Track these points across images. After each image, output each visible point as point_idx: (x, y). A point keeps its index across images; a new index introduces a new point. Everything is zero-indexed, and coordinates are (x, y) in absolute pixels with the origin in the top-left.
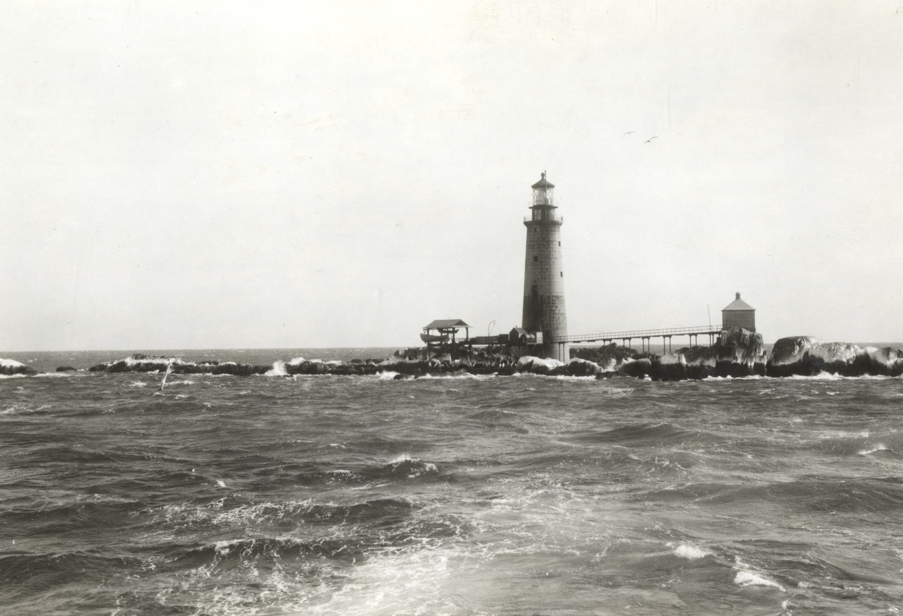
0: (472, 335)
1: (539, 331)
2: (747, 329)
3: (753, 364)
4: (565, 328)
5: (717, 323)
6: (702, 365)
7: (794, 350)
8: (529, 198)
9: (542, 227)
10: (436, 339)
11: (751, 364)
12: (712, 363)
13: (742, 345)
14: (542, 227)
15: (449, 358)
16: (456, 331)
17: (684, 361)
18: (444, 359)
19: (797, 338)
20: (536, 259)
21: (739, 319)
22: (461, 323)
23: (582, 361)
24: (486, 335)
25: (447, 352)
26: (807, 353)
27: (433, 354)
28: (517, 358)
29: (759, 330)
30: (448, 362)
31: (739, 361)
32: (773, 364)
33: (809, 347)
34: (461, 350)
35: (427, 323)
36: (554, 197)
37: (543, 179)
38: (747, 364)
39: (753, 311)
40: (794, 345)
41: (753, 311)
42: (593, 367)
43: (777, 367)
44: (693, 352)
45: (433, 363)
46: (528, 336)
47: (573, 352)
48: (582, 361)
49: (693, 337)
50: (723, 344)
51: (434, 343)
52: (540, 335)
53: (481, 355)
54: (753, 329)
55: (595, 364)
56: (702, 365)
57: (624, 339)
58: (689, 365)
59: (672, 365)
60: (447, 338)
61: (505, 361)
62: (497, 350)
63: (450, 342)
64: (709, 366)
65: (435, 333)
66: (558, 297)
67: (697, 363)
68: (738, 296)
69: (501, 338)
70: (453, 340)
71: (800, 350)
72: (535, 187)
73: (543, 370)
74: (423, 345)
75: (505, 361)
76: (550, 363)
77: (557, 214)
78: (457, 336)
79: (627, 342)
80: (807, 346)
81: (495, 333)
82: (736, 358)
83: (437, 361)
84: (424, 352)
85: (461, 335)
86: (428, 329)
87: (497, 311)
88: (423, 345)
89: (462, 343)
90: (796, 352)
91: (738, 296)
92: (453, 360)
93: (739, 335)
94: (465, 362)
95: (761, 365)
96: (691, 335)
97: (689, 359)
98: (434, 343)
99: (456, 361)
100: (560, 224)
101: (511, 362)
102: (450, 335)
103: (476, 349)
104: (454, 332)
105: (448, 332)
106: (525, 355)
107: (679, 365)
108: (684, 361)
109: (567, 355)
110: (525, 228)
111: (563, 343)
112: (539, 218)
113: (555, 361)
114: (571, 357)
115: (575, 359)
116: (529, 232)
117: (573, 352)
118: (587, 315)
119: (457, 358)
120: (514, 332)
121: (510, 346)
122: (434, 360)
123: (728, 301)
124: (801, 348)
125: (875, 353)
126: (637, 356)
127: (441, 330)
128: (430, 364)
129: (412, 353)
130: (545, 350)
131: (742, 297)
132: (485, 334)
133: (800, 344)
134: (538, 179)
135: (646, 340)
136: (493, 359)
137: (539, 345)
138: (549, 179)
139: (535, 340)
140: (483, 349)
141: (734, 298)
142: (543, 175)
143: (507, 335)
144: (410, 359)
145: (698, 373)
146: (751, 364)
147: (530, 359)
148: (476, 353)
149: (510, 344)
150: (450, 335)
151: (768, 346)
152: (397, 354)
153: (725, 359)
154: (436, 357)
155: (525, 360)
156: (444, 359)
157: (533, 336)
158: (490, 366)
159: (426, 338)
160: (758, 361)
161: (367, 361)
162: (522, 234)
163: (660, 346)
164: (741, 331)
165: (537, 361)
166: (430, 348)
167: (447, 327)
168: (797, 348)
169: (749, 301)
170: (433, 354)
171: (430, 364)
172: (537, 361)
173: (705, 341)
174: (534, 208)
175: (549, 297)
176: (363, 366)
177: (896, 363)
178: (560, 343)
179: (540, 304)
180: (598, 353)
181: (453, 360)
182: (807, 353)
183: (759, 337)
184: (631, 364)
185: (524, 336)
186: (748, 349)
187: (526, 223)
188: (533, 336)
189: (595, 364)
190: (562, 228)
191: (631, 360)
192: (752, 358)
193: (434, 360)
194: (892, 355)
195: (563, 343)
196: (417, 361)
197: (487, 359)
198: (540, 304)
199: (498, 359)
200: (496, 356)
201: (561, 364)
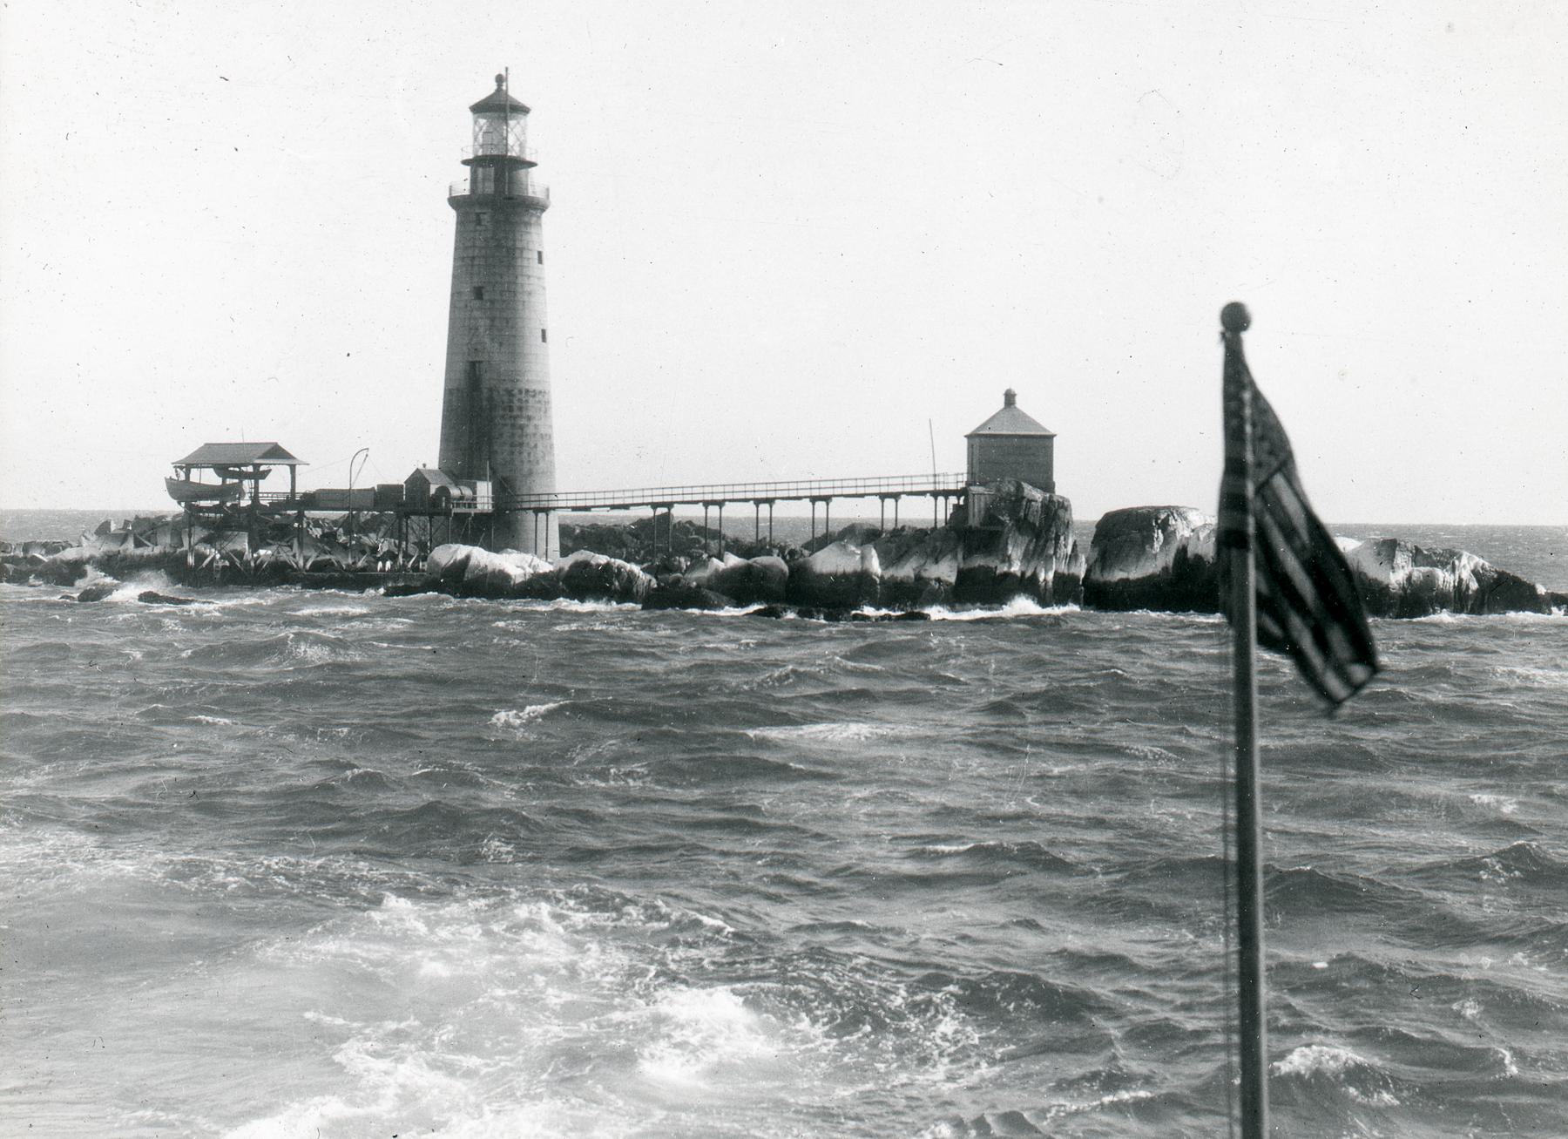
0: (306, 485)
1: (482, 478)
2: (1035, 485)
3: (1051, 575)
4: (549, 473)
5: (954, 467)
6: (918, 578)
7: (1150, 540)
8: (465, 137)
9: (496, 212)
10: (210, 492)
11: (1046, 576)
12: (945, 571)
13: (1023, 525)
14: (496, 212)
15: (242, 543)
16: (264, 475)
17: (875, 566)
18: (230, 547)
19: (1158, 510)
20: (478, 293)
21: (1011, 462)
22: (276, 453)
23: (603, 559)
24: (343, 485)
25: (240, 528)
26: (1183, 550)
27: (200, 533)
28: (424, 549)
29: (1063, 487)
30: (240, 554)
31: (1016, 568)
32: (1097, 576)
33: (1187, 533)
34: (274, 523)
35: (184, 453)
36: (522, 138)
37: (499, 90)
38: (1035, 576)
39: (1050, 438)
40: (1151, 530)
41: (1050, 438)
42: (631, 577)
43: (1106, 584)
44: (898, 542)
45: (200, 557)
46: (455, 492)
47: (572, 538)
48: (603, 559)
49: (889, 502)
50: (974, 521)
51: (203, 503)
52: (484, 489)
53: (329, 538)
54: (1048, 486)
55: (636, 569)
56: (918, 578)
57: (707, 504)
58: (887, 575)
59: (845, 575)
60: (237, 491)
61: (392, 556)
62: (366, 528)
63: (245, 502)
64: (938, 580)
65: (210, 478)
66: (535, 394)
67: (906, 571)
68: (1010, 398)
69: (384, 496)
70: (255, 498)
71: (1166, 542)
72: (479, 109)
73: (495, 586)
74: (173, 508)
75: (392, 556)
76: (514, 564)
77: (535, 182)
78: (264, 486)
79: (714, 511)
80: (1182, 531)
81: (369, 479)
82: (1007, 560)
83: (211, 553)
84: (177, 528)
85: (276, 483)
86: (187, 466)
87: (381, 428)
88: (173, 508)
89: (277, 506)
90: (1157, 546)
91: (1010, 398)
92: (254, 549)
93: (1018, 498)
94: (285, 556)
95: (1073, 579)
96: (883, 496)
97: (888, 560)
98: (203, 503)
99: (262, 552)
100: (543, 208)
101: (407, 556)
102: (247, 485)
103: (317, 523)
104: (259, 475)
105: (243, 476)
106: (444, 541)
107: (863, 577)
108: (875, 566)
109: (555, 544)
110: (451, 216)
111: (546, 510)
112: (490, 188)
113: (529, 557)
114: (565, 552)
115: (582, 555)
116: (461, 223)
117: (572, 538)
118: (602, 446)
119: (267, 545)
120: (418, 480)
121: (407, 516)
122: (201, 548)
123: (982, 410)
124: (1169, 536)
125: (1357, 552)
126: (745, 551)
127: (222, 470)
128: (191, 560)
129: (146, 528)
130: (499, 528)
131: (1020, 403)
132: (339, 482)
133: (1164, 526)
134: (487, 89)
135: (821, 505)
136: (362, 550)
137: (482, 517)
138: (517, 91)
139: (472, 502)
140: (335, 522)
141: (1002, 399)
142: (500, 79)
143: (398, 488)
144: (138, 544)
145: (907, 597)
146: (1046, 576)
147: (461, 551)
148: (317, 532)
149: (406, 505)
150: (247, 485)
151: (1084, 525)
152: (103, 530)
153: (978, 561)
154: (208, 541)
155: (448, 554)
156: (230, 547)
157: (467, 492)
158: (352, 569)
159: (179, 490)
160: (1063, 569)
161: (26, 547)
162: (439, 234)
163: (803, 521)
164: (1019, 488)
165: (482, 557)
166: (193, 517)
167: (240, 463)
168: (1159, 535)
169: (1039, 411)
170: (200, 533)
171: (191, 560)
172: (482, 557)
173: (923, 513)
174: (475, 163)
175: (510, 393)
176: (14, 560)
177: (1409, 578)
178: (537, 511)
179: (487, 410)
180: (627, 538)
181: (254, 549)
182: (1183, 550)
183: (1064, 506)
184: (734, 571)
185: (443, 491)
186: (1038, 537)
187: (455, 202)
188: (467, 492)
189: (636, 569)
190: (546, 217)
191: (733, 560)
192: (1048, 559)
193: (201, 548)
194: (1401, 559)
195: (546, 510)
196: (157, 550)
197: (345, 548)
198: (487, 410)
199: (374, 549)
200: (370, 539)
201: (545, 567)
